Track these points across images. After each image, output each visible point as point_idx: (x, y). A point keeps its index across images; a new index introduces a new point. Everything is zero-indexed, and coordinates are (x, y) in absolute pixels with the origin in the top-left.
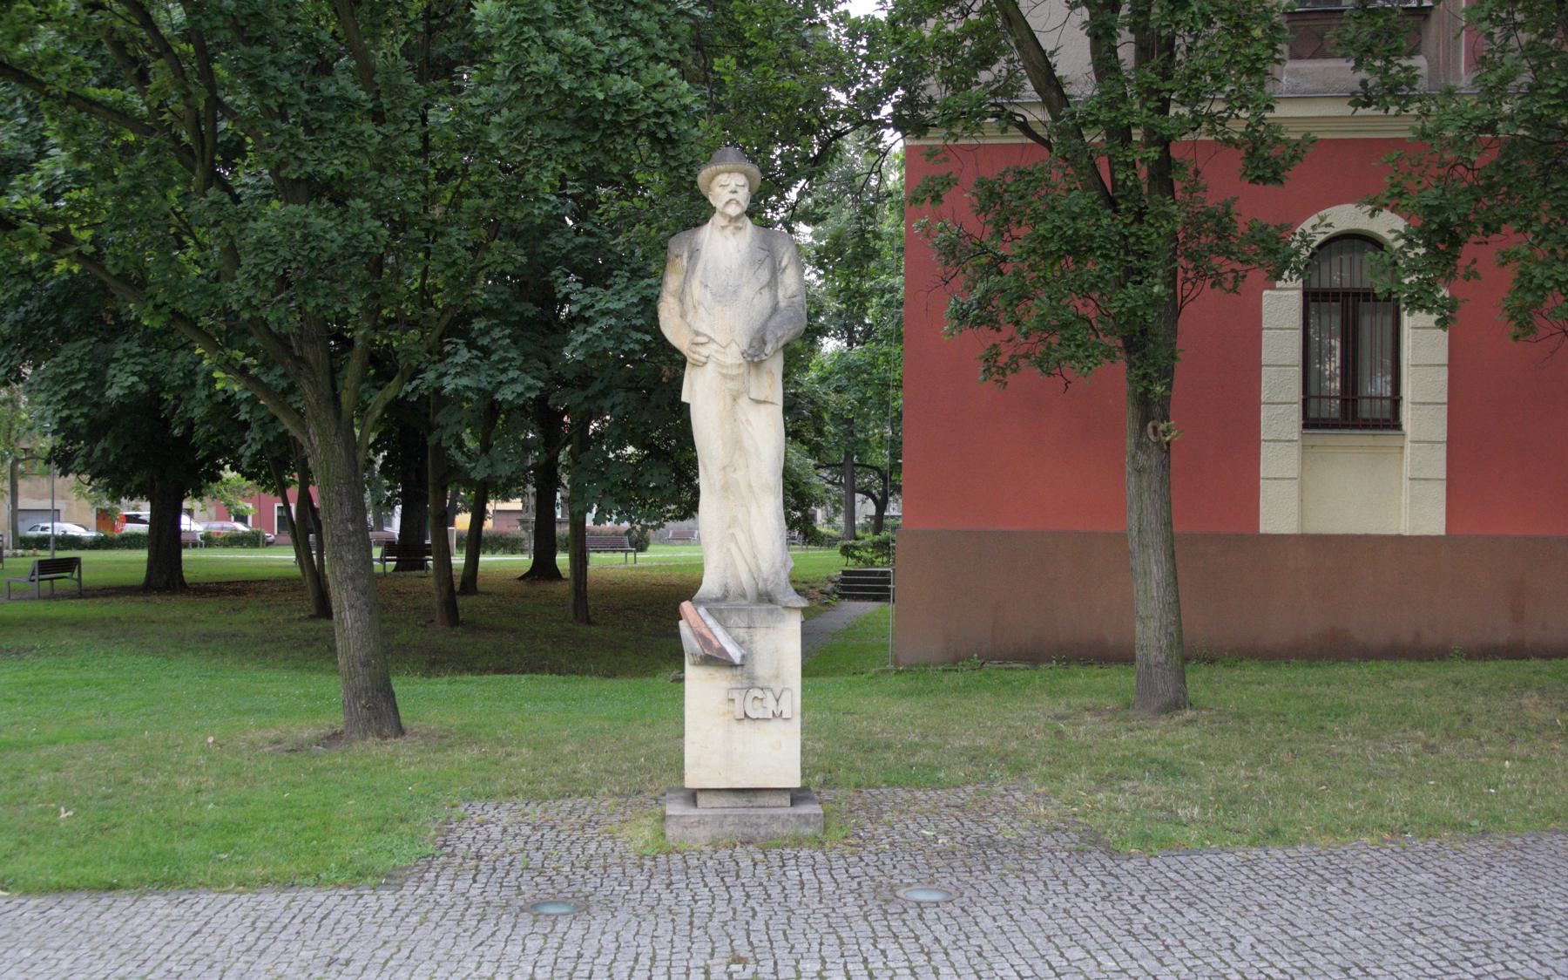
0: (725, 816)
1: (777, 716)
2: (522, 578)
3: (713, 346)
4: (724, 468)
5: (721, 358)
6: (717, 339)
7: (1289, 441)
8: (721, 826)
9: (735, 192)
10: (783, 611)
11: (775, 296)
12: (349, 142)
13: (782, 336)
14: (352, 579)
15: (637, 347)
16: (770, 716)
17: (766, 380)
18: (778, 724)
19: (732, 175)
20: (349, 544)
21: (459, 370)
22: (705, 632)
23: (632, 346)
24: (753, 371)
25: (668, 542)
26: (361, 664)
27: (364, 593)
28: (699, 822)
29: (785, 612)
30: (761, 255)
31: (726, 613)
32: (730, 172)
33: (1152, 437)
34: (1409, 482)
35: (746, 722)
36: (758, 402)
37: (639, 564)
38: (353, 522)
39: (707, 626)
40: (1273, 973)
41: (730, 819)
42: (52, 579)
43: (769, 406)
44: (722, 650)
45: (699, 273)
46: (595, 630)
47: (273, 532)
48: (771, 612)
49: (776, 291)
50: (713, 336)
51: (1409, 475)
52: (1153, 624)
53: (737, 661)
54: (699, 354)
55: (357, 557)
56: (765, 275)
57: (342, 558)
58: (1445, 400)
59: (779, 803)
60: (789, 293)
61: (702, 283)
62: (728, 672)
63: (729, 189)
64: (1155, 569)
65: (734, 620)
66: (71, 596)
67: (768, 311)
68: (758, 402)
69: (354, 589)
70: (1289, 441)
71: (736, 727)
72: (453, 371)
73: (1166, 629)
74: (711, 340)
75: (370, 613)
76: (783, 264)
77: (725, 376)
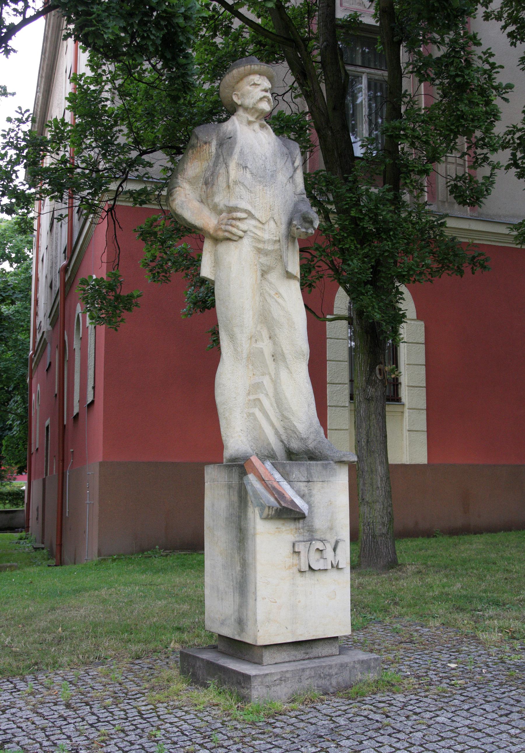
0: (303, 670)
5: (259, 233)
6: (257, 215)
7: (343, 407)
16: (330, 567)
18: (333, 574)
19: (262, 77)
33: (378, 376)
34: (407, 433)
35: (309, 574)
40: (488, 748)
41: (307, 672)
48: (325, 467)
50: (253, 212)
51: (407, 428)
52: (378, 506)
54: (237, 228)
58: (425, 385)
64: (379, 468)
70: (343, 407)
71: (300, 580)
73: (387, 510)
74: (251, 215)
77: (259, 251)
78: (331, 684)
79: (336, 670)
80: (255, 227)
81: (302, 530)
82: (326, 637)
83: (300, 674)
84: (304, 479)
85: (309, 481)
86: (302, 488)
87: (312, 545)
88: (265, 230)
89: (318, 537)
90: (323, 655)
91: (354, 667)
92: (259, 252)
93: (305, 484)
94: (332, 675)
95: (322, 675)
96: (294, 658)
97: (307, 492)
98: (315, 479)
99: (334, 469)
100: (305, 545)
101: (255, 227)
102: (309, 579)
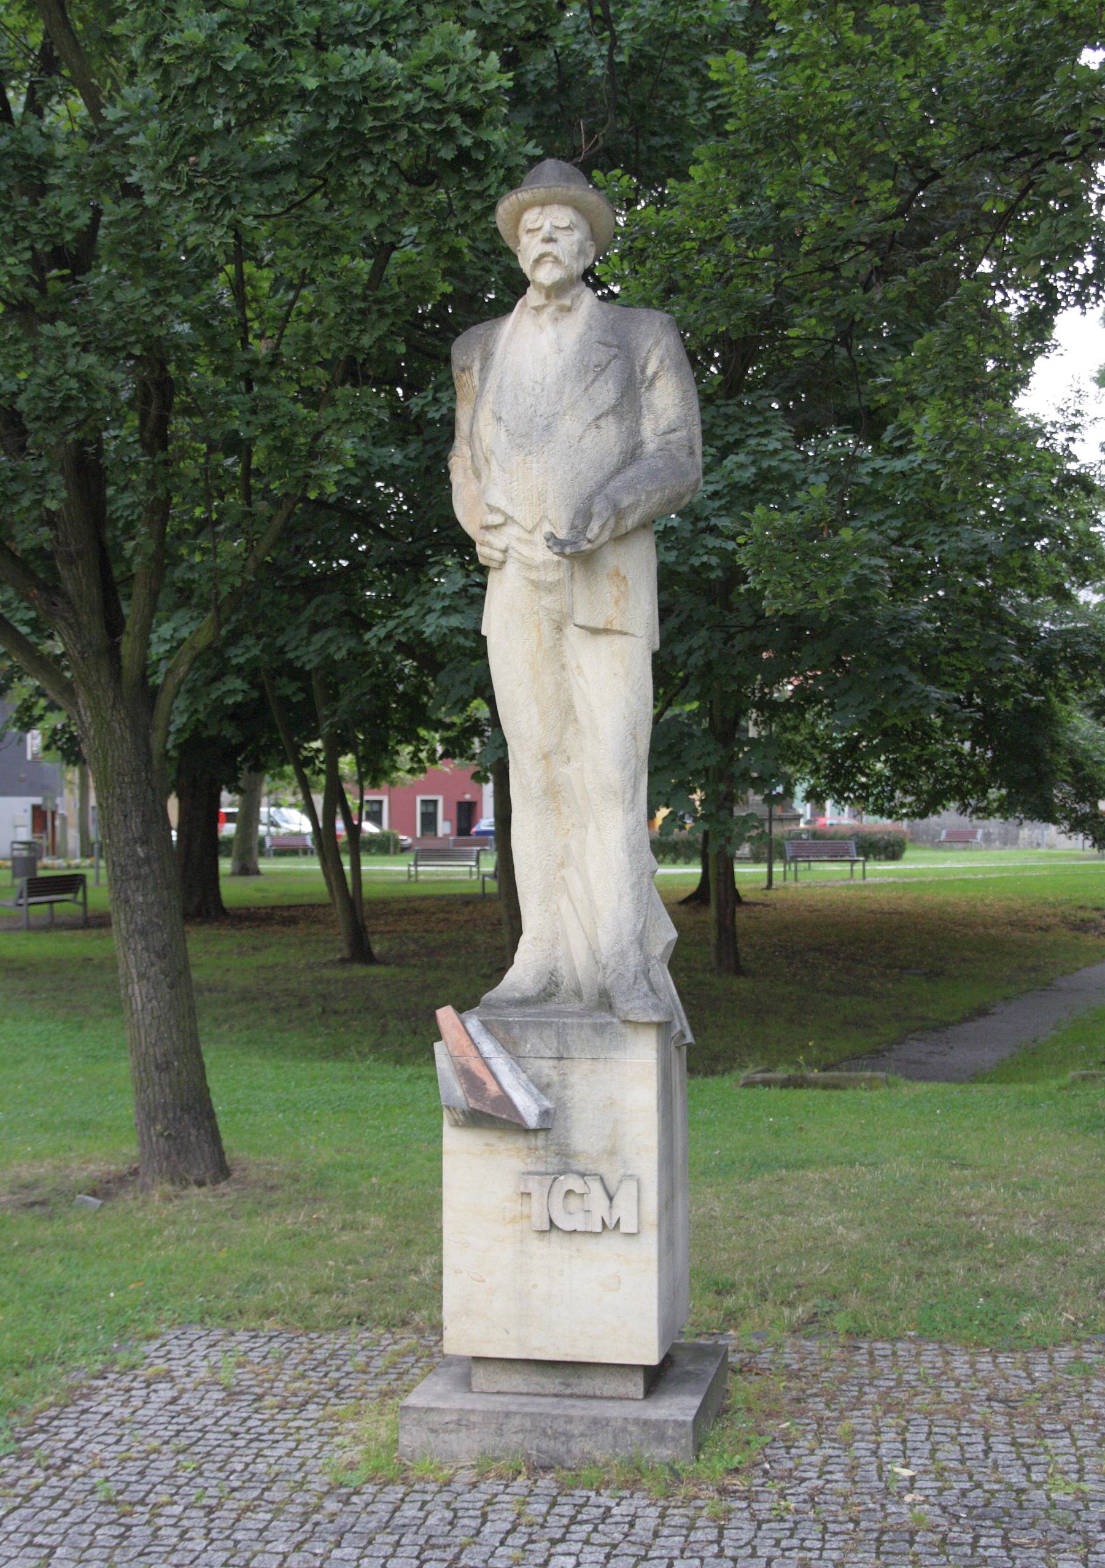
0: (507, 1415)
1: (611, 1228)
2: (685, 901)
3: (512, 531)
4: (546, 757)
5: (525, 551)
6: (518, 516)
8: (500, 1431)
9: (549, 240)
10: (623, 1029)
11: (634, 432)
12: (34, 228)
13: (633, 506)
14: (143, 933)
15: (714, 561)
16: (598, 1228)
17: (608, 590)
18: (612, 1244)
19: (548, 210)
20: (137, 878)
21: (447, 603)
22: (475, 1065)
23: (705, 559)
24: (579, 575)
25: (937, 845)
26: (157, 1067)
27: (161, 956)
28: (458, 1423)
29: (627, 1031)
30: (601, 355)
31: (516, 1031)
32: (543, 204)
36: (595, 631)
37: (869, 879)
38: (145, 842)
39: (480, 1054)
41: (516, 1421)
42: (51, 902)
43: (618, 640)
44: (505, 1100)
45: (489, 397)
46: (742, 984)
47: (412, 834)
48: (600, 1029)
49: (637, 421)
50: (510, 512)
53: (532, 1121)
55: (151, 898)
56: (607, 392)
57: (127, 901)
59: (622, 1391)
60: (663, 424)
61: (494, 413)
62: (521, 1142)
63: (541, 235)
65: (531, 1043)
66: (72, 925)
67: (612, 460)
68: (595, 631)
69: (146, 949)
71: (537, 1246)
72: (438, 605)
74: (508, 520)
75: (172, 986)
76: (650, 371)
77: (536, 585)
78: (569, 1451)
79: (582, 1428)
80: (519, 539)
81: (542, 1152)
82: (596, 1360)
83: (501, 1420)
84: (549, 1054)
85: (560, 1058)
86: (546, 1071)
87: (556, 1183)
88: (535, 544)
89: (581, 1168)
90: (605, 1394)
91: (624, 1430)
92: (537, 587)
93: (551, 1063)
94: (573, 1436)
95: (549, 1432)
96: (539, 1390)
97: (556, 1078)
98: (576, 1055)
99: (621, 1035)
100: (541, 1183)
101: (519, 539)
102: (555, 1248)
